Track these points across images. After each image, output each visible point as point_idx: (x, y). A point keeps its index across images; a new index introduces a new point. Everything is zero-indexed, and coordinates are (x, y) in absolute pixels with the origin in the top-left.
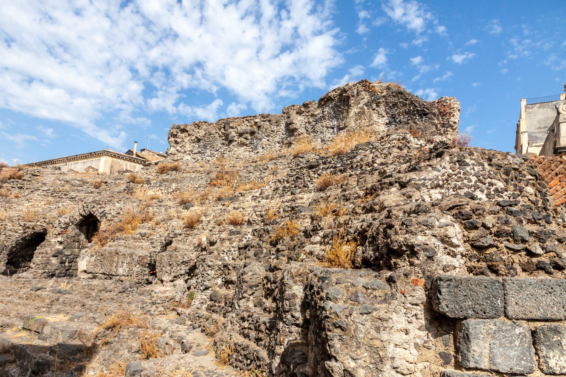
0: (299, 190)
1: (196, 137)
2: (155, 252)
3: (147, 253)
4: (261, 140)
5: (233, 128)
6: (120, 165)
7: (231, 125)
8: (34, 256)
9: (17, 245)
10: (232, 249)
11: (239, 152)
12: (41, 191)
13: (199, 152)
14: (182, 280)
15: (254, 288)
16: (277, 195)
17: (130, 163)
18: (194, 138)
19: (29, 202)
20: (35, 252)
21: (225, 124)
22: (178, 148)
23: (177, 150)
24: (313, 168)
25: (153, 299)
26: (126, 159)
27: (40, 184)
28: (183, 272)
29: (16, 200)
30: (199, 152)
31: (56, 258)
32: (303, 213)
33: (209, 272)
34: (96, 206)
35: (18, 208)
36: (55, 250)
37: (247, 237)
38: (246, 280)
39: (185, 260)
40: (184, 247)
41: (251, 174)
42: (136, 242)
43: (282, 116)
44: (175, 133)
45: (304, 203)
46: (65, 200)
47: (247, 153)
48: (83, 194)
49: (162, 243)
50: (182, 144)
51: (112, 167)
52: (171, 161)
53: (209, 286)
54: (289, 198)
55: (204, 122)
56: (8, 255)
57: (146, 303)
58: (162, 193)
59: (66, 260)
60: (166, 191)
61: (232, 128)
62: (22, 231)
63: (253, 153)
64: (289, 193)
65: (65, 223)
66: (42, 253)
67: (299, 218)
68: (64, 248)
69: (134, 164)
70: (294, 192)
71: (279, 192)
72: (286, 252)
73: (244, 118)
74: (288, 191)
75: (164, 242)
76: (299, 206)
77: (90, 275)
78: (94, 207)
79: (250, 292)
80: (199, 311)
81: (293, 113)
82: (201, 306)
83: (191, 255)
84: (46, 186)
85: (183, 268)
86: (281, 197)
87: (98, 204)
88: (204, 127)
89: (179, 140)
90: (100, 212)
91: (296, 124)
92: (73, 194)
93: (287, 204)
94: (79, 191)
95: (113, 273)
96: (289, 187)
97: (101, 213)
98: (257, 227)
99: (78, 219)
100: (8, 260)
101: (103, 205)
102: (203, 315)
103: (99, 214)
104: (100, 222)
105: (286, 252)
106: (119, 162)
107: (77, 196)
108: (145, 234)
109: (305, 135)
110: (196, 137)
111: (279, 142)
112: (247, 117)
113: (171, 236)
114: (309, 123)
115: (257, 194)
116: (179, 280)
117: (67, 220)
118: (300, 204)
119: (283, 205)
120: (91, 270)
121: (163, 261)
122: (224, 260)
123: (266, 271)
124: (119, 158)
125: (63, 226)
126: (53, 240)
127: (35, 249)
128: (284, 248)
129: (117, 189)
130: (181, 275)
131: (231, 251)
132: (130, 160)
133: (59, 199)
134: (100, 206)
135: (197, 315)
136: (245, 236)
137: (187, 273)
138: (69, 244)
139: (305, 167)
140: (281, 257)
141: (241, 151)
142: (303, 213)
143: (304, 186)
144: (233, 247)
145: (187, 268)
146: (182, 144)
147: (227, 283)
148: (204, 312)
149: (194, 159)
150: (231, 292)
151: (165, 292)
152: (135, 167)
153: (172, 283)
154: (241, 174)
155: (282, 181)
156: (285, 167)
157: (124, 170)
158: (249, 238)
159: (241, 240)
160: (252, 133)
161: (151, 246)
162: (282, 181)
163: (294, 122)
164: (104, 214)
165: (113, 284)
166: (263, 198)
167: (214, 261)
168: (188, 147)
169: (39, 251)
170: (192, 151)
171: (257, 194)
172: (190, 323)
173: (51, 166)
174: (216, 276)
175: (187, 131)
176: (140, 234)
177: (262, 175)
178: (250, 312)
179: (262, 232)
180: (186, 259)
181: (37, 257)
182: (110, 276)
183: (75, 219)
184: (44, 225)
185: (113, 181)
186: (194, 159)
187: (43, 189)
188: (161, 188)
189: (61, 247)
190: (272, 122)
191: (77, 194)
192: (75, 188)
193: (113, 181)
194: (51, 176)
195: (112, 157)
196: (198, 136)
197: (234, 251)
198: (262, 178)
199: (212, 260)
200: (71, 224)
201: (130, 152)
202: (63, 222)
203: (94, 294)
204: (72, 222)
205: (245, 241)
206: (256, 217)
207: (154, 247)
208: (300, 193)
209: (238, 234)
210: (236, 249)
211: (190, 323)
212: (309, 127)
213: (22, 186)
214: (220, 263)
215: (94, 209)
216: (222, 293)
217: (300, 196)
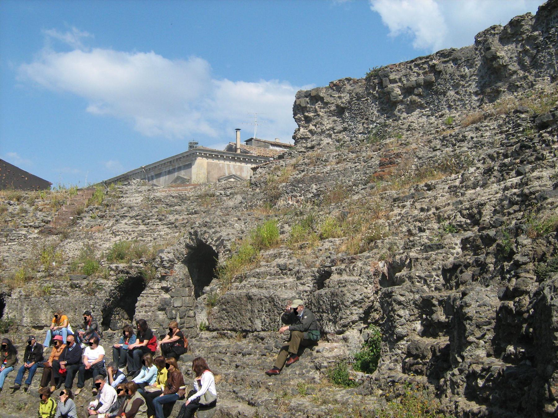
0: (530, 166)
1: (337, 106)
2: (306, 292)
3: (294, 294)
4: (444, 94)
5: (396, 82)
6: (220, 168)
7: (392, 77)
8: (136, 311)
9: (111, 296)
10: (434, 274)
11: (410, 119)
12: (129, 218)
13: (345, 129)
14: (355, 331)
15: (485, 327)
16: (493, 179)
17: (232, 163)
18: (333, 108)
19: (116, 235)
20: (137, 304)
21: (378, 79)
22: (312, 127)
23: (311, 131)
24: (547, 127)
25: (316, 361)
26: (227, 159)
27: (125, 209)
28: (355, 317)
29: (100, 235)
30: (345, 129)
31: (164, 312)
32: (550, 200)
33: (401, 312)
34: (208, 230)
35: (104, 246)
36: (161, 300)
37: (454, 251)
38: (470, 314)
39: (356, 298)
40: (352, 278)
41: (438, 153)
42: (274, 279)
43: (476, 49)
44: (303, 105)
45: (545, 185)
46: (161, 227)
47: (424, 119)
48: (185, 217)
49: (315, 276)
50: (316, 121)
51: (208, 173)
52: (303, 150)
53: (404, 334)
54: (516, 180)
55: (347, 79)
56: (102, 311)
57: (306, 367)
58: (297, 202)
59: (176, 315)
60: (302, 197)
61: (394, 81)
62: (115, 277)
63: (433, 119)
64: (513, 173)
65: (170, 261)
66: (146, 306)
67: (545, 208)
68: (172, 297)
69: (238, 164)
70: (521, 169)
71: (495, 173)
72: (531, 266)
73: (412, 61)
74: (512, 170)
75: (317, 275)
76: (537, 191)
77: (215, 334)
78: (205, 232)
79: (478, 334)
80: (393, 374)
81: (495, 43)
82: (395, 365)
83: (365, 290)
84: (134, 210)
85: (354, 312)
86: (499, 181)
87: (210, 227)
88: (348, 87)
89: (311, 115)
90: (215, 239)
91: (503, 58)
92: (171, 218)
93: (514, 191)
94: (178, 213)
95: (248, 328)
96: (511, 164)
97: (216, 241)
98: (469, 234)
99: (185, 252)
100: (103, 318)
101: (218, 229)
102: (401, 378)
103: (213, 243)
104: (217, 255)
105: (531, 266)
106: (217, 165)
107: (176, 220)
108: (285, 265)
109: (521, 73)
110: (337, 106)
111: (476, 94)
112: (416, 60)
113: (328, 264)
114: (525, 52)
115: (457, 183)
116: (351, 330)
117: (171, 256)
118: (538, 188)
119: (508, 193)
120: (217, 326)
121: (321, 303)
122: (423, 291)
123: (501, 299)
124: (217, 157)
125: (168, 265)
126: (156, 287)
127: (136, 301)
128: (526, 259)
129: (231, 203)
130: (354, 322)
131: (432, 276)
132: (233, 159)
133: (153, 227)
134: (213, 230)
135: (391, 379)
136: (452, 251)
137: (361, 319)
138: (178, 291)
139: (532, 128)
140: (523, 274)
141: (416, 118)
142: (550, 200)
143: (537, 159)
144: (434, 270)
145: (361, 311)
146: (316, 121)
147: (431, 329)
148: (399, 373)
149: (338, 141)
150: (443, 341)
151: (331, 350)
152: (241, 169)
153: (341, 336)
154: (421, 154)
155: (495, 155)
156: (494, 132)
157: (227, 175)
158: (458, 254)
159: (445, 258)
160: (428, 85)
161: (298, 282)
162: (495, 155)
163: (498, 54)
164: (221, 242)
165: (250, 344)
166: (467, 187)
167: (407, 293)
168: (328, 123)
169: (141, 303)
170: (333, 129)
171: (457, 183)
172: (381, 392)
173: (134, 181)
174: (413, 318)
175: (322, 99)
176: (278, 266)
177: (457, 151)
178: (483, 363)
179: (479, 242)
180: (358, 297)
181: (140, 312)
182: (245, 333)
183: (181, 253)
184: (141, 265)
185: (223, 192)
186: (338, 141)
187: (131, 215)
188: (295, 193)
189: (167, 296)
190: (459, 62)
191: (177, 216)
192: (172, 208)
193: (223, 192)
194: (137, 195)
195: (207, 157)
196: (339, 102)
197: (437, 276)
198: (458, 157)
199: (402, 292)
200: (176, 261)
201: (231, 149)
202: (166, 258)
203: (226, 359)
204: (178, 258)
205: (451, 259)
206: (464, 220)
207: (303, 284)
208: (533, 170)
209: (438, 249)
210: (440, 272)
211: (381, 392)
212: (527, 61)
213: (103, 214)
214: (417, 296)
215: (207, 235)
216: (427, 342)
217: (536, 174)
